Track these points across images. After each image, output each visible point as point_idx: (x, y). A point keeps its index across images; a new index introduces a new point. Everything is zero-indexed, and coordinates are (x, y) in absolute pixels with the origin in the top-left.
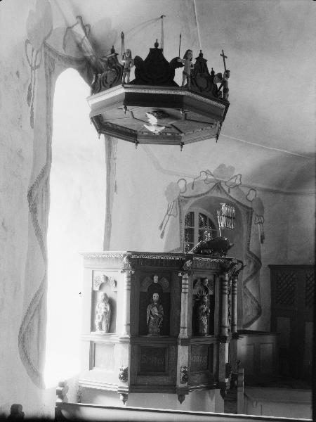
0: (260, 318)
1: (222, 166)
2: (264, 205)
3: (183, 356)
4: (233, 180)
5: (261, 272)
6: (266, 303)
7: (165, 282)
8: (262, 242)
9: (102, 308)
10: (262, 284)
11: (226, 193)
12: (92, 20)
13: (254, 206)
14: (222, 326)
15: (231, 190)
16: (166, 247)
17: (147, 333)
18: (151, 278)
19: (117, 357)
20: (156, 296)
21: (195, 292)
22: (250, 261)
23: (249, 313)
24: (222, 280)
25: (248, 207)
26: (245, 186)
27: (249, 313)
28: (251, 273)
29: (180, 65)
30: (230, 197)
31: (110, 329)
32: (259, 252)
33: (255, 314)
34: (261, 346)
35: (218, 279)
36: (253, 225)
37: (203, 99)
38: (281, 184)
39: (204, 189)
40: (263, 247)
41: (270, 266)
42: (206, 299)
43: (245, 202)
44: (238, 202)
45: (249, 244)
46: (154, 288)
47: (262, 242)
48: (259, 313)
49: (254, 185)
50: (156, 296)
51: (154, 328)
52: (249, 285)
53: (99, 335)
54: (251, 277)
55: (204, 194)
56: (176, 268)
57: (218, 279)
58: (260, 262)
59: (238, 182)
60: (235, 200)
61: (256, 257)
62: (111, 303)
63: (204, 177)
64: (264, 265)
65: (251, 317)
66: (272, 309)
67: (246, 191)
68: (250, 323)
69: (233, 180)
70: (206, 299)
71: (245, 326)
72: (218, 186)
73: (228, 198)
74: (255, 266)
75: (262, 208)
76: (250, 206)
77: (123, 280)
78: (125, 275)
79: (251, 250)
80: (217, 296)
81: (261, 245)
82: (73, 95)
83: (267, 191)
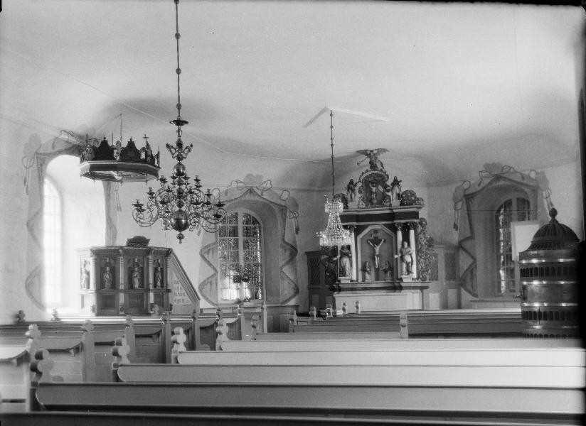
0: (297, 297)
1: (249, 176)
2: (298, 202)
3: (122, 298)
4: (264, 185)
5: (298, 258)
6: (304, 283)
7: (112, 261)
8: (297, 233)
9: (85, 276)
10: (298, 268)
11: (259, 196)
12: (69, 128)
13: (288, 204)
14: (148, 284)
15: (264, 193)
16: (106, 243)
17: (104, 287)
18: (105, 260)
19: (91, 300)
20: (108, 269)
21: (155, 266)
22: (285, 250)
23: (286, 292)
24: (148, 259)
25: (282, 206)
26: (277, 188)
27: (286, 292)
28: (288, 259)
29: (115, 149)
30: (264, 198)
31: (88, 288)
32: (295, 242)
33: (292, 292)
34: (281, 315)
35: (145, 259)
36: (287, 219)
37: (131, 164)
38: (312, 183)
39: (237, 194)
40: (298, 237)
41: (308, 254)
42: (159, 269)
43: (279, 202)
44: (271, 202)
45: (284, 236)
46: (107, 264)
47: (297, 233)
48: (297, 291)
49: (288, 186)
50: (108, 269)
51: (107, 285)
52: (287, 270)
53: (84, 291)
54: (288, 263)
55: (236, 199)
56: (242, 262)
57: (145, 259)
58: (296, 250)
59: (269, 186)
60: (266, 200)
61: (292, 247)
62: (88, 273)
63: (235, 185)
64: (301, 252)
65: (288, 297)
66: (309, 289)
67: (279, 192)
68: (289, 300)
69: (264, 185)
70: (159, 269)
71: (282, 303)
72: (251, 191)
73: (262, 200)
74: (291, 254)
75: (296, 205)
76: (283, 204)
77: (91, 260)
78: (92, 258)
79: (286, 240)
80: (145, 267)
81: (296, 235)
82: (69, 167)
83: (299, 190)
